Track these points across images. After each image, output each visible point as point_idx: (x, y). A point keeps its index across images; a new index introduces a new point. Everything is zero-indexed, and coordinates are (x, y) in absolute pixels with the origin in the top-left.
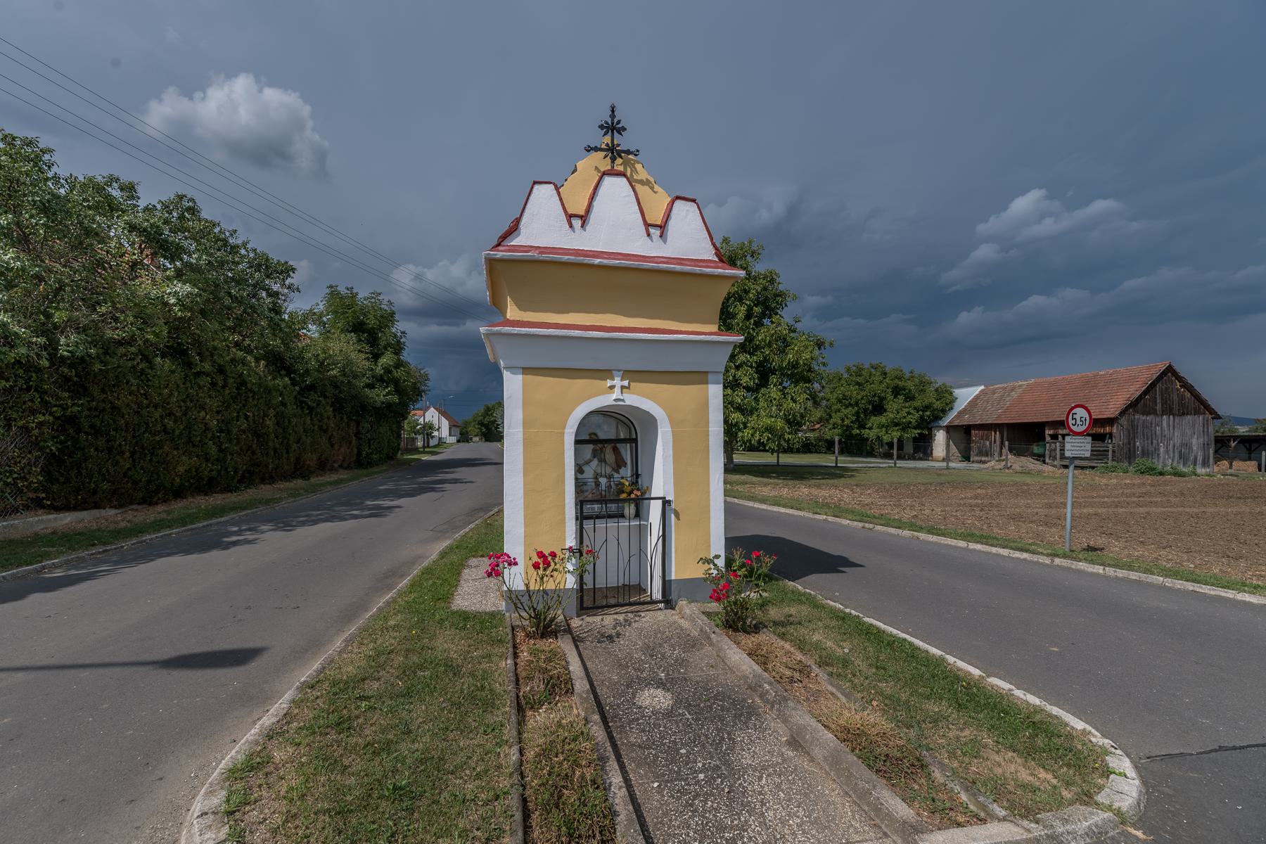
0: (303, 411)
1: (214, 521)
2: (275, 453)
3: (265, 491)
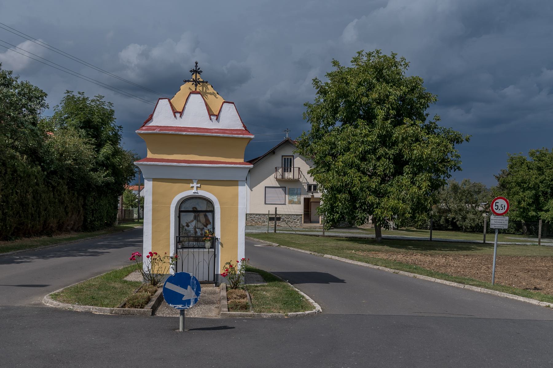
0: (49, 189)
1: (5, 254)
2: (32, 217)
3: (26, 241)
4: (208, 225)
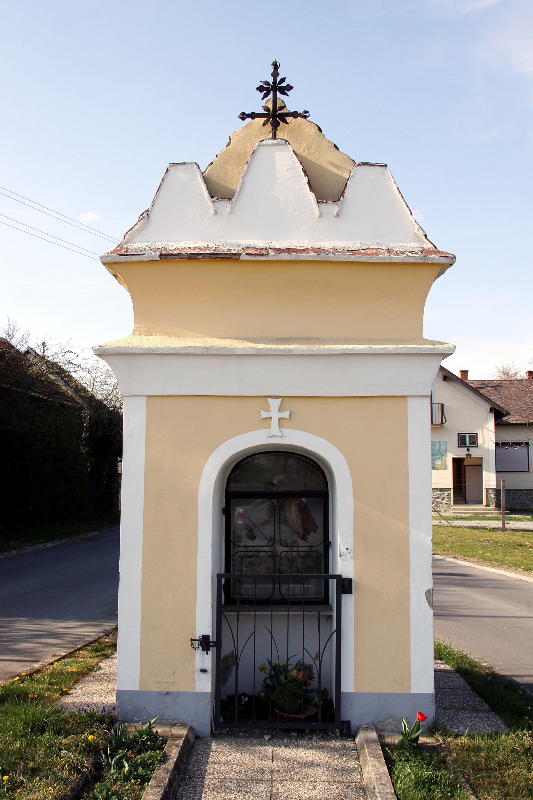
4: (309, 534)
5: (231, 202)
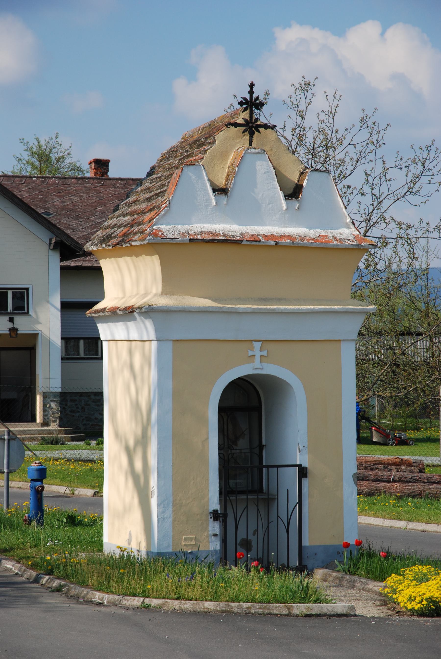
5: (226, 196)
